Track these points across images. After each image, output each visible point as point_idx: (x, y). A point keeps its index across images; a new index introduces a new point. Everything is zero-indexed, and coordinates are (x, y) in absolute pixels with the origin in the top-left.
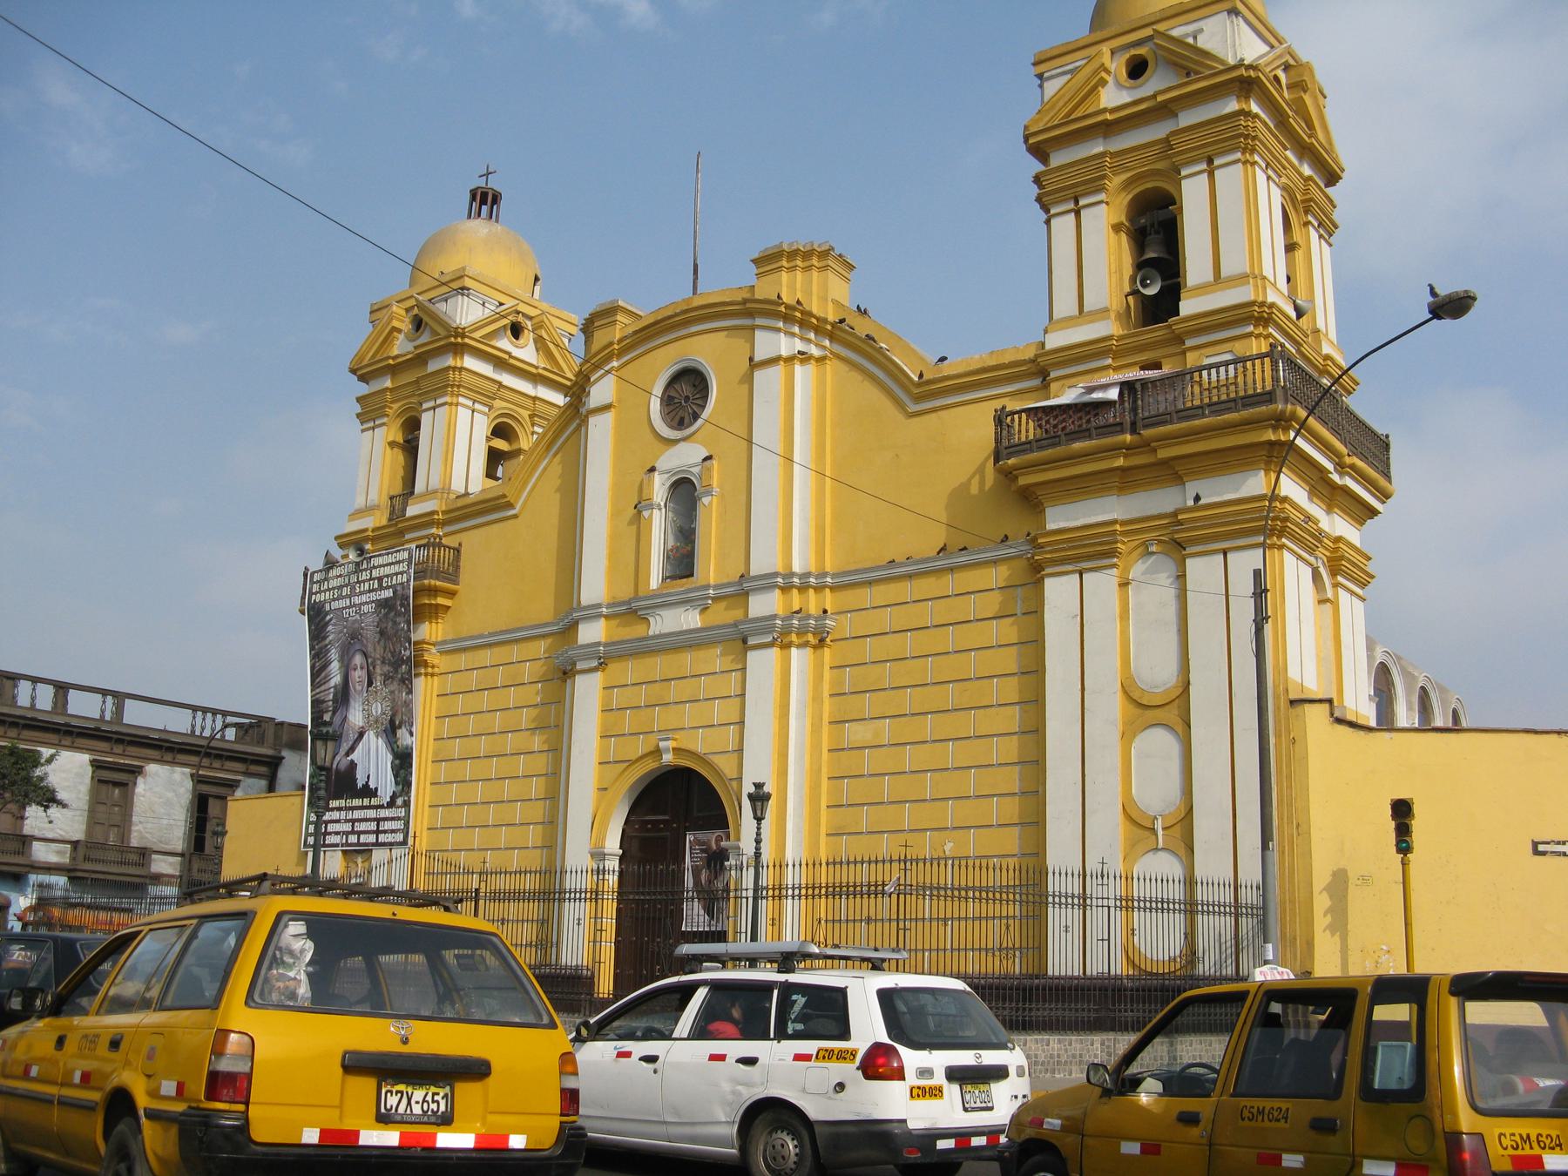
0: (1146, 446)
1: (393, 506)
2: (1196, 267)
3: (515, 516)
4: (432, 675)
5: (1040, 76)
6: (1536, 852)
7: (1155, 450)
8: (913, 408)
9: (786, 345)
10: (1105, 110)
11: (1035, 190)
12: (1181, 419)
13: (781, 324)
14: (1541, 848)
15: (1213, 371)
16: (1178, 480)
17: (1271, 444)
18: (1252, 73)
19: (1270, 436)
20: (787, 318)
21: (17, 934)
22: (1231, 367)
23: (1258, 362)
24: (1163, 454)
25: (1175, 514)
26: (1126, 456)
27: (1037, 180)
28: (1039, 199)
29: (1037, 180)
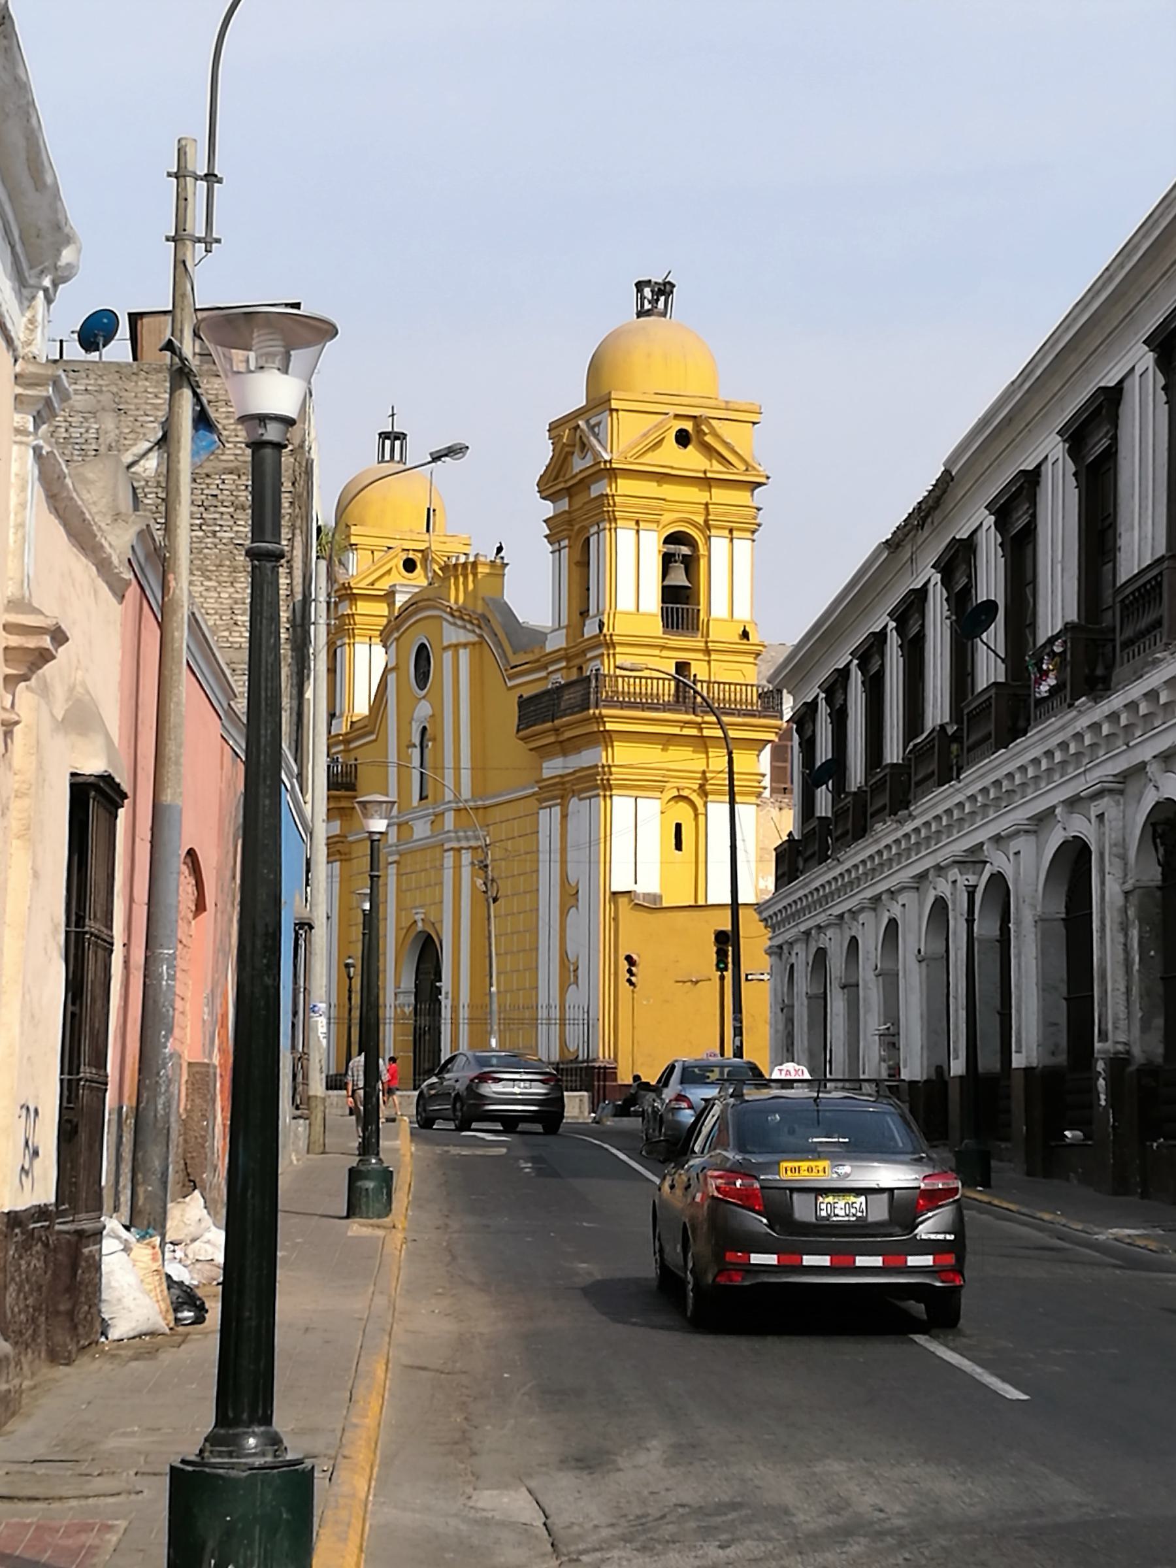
8: (509, 684)
14: (750, 977)
18: (608, 466)
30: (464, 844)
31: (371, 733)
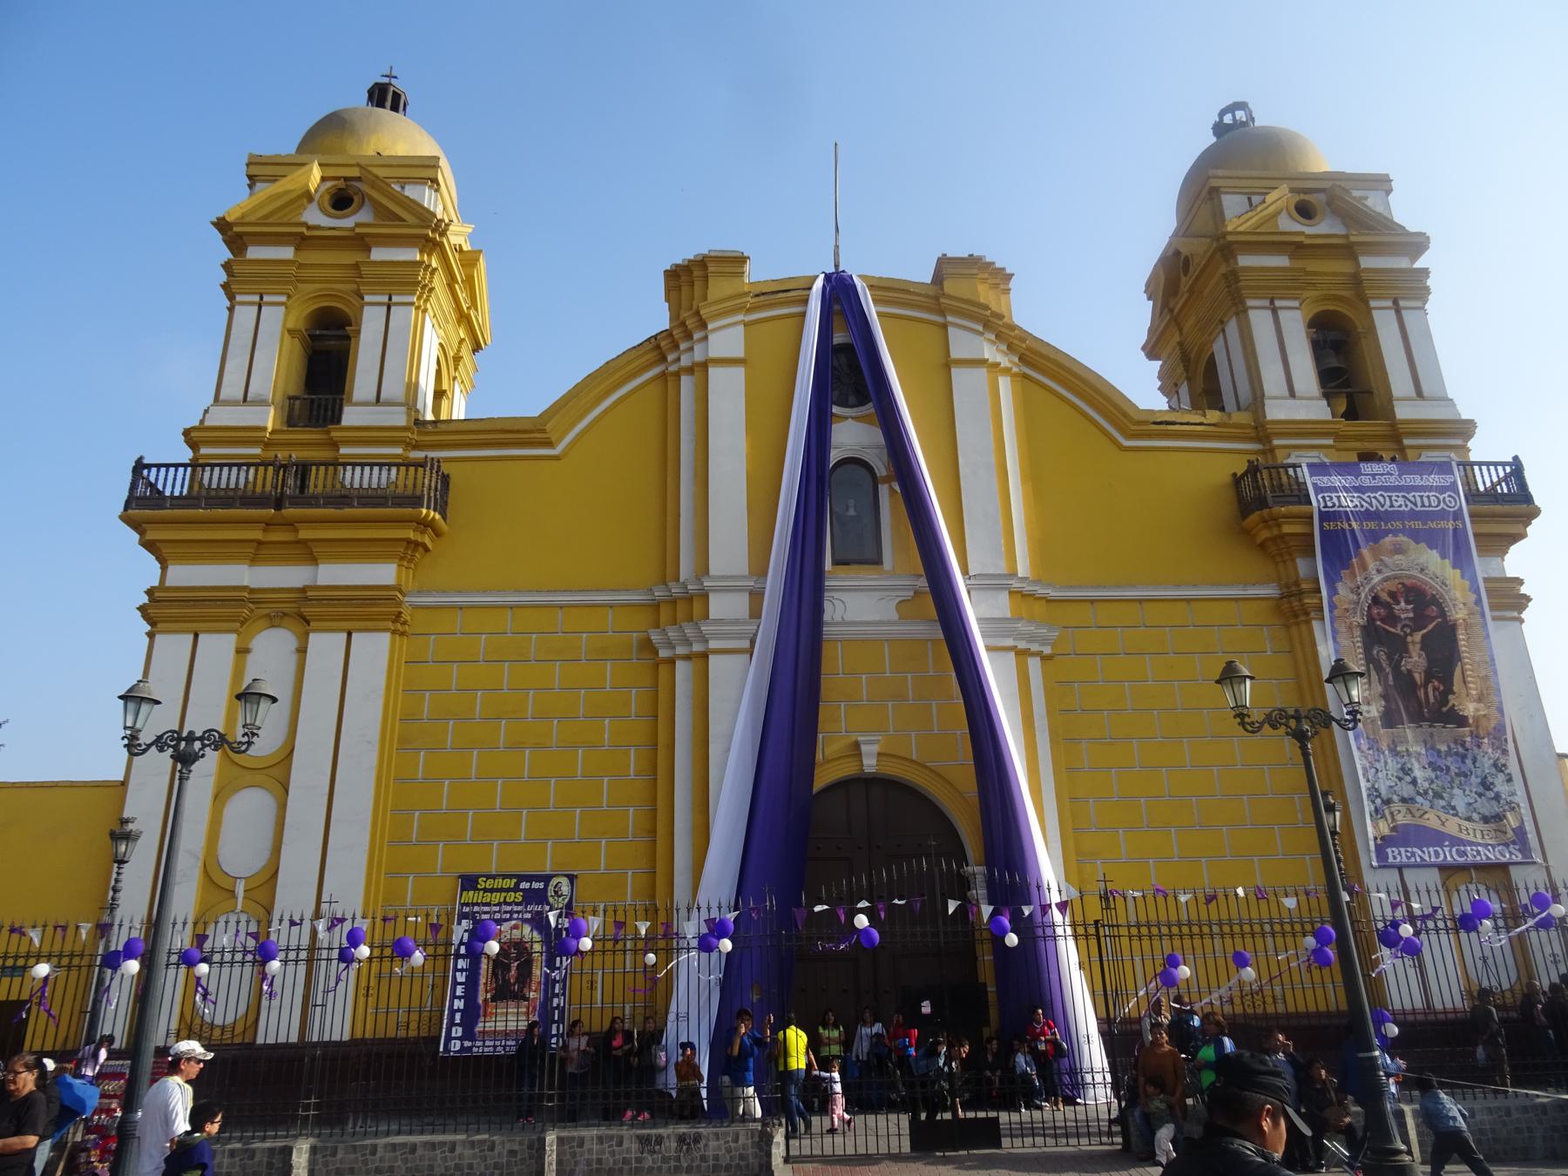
0: (291, 525)
1: (291, 409)
2: (362, 382)
3: (557, 458)
4: (402, 634)
5: (250, 177)
6: (12, 930)
7: (297, 531)
9: (990, 352)
10: (305, 224)
11: (223, 277)
12: (395, 505)
13: (980, 328)
15: (394, 470)
16: (313, 560)
17: (409, 541)
19: (411, 535)
20: (987, 325)
21: (142, 964)
22: (252, 470)
23: (403, 469)
24: (304, 534)
25: (303, 590)
26: (265, 530)
27: (227, 266)
28: (225, 286)
29: (227, 266)
30: (680, 650)
31: (548, 444)
